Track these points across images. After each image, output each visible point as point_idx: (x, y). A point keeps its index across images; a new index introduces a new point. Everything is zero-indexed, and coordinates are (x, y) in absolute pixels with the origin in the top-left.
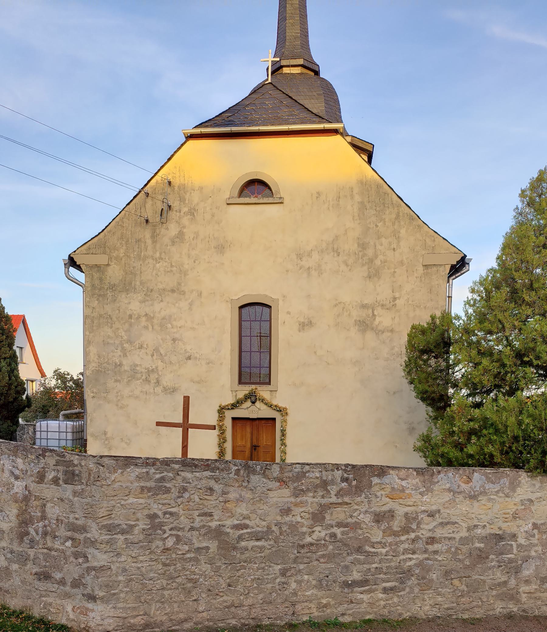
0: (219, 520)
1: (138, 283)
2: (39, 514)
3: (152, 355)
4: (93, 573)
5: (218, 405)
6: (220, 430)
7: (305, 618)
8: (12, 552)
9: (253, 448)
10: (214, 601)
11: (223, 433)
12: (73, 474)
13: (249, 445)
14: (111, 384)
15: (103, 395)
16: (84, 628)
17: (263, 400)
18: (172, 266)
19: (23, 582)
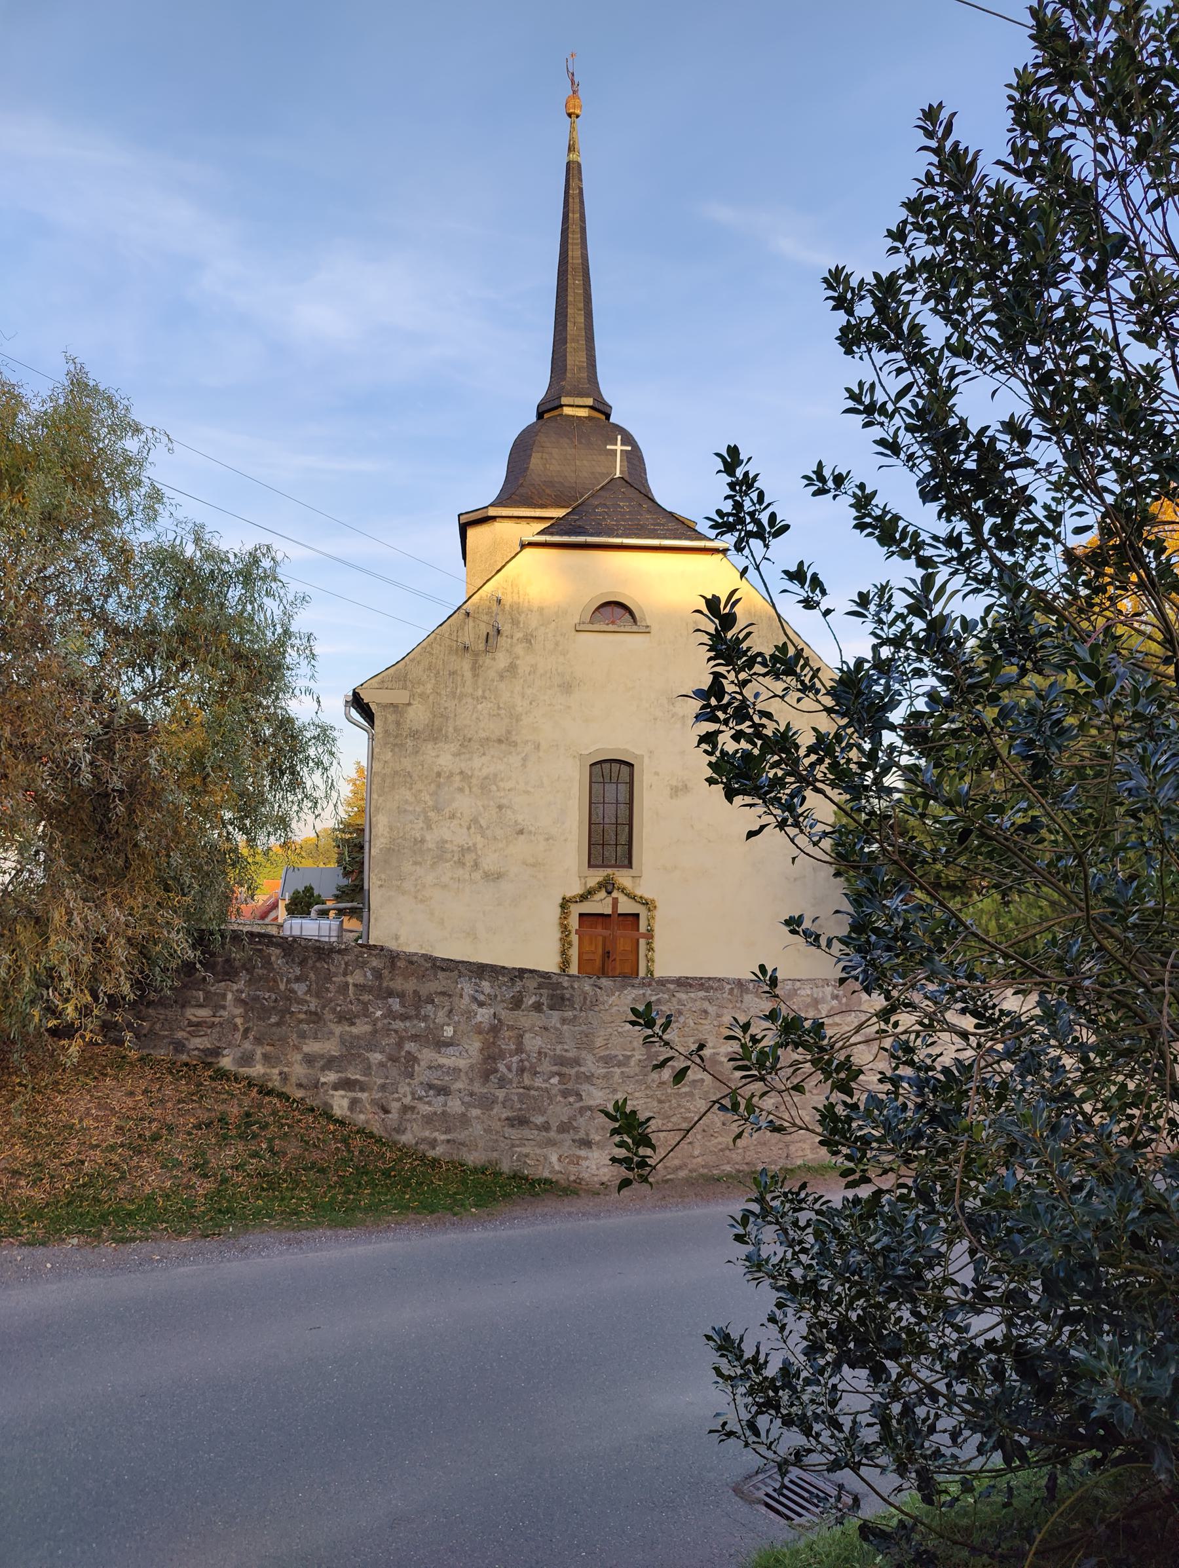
0: (714, 1048)
1: (451, 730)
2: (513, 1047)
3: (469, 828)
4: (589, 1113)
7: (799, 1162)
8: (471, 1095)
10: (708, 1144)
12: (563, 998)
13: (600, 951)
14: (407, 867)
15: (395, 883)
16: (575, 1181)
17: (623, 890)
18: (499, 708)
19: (488, 1130)
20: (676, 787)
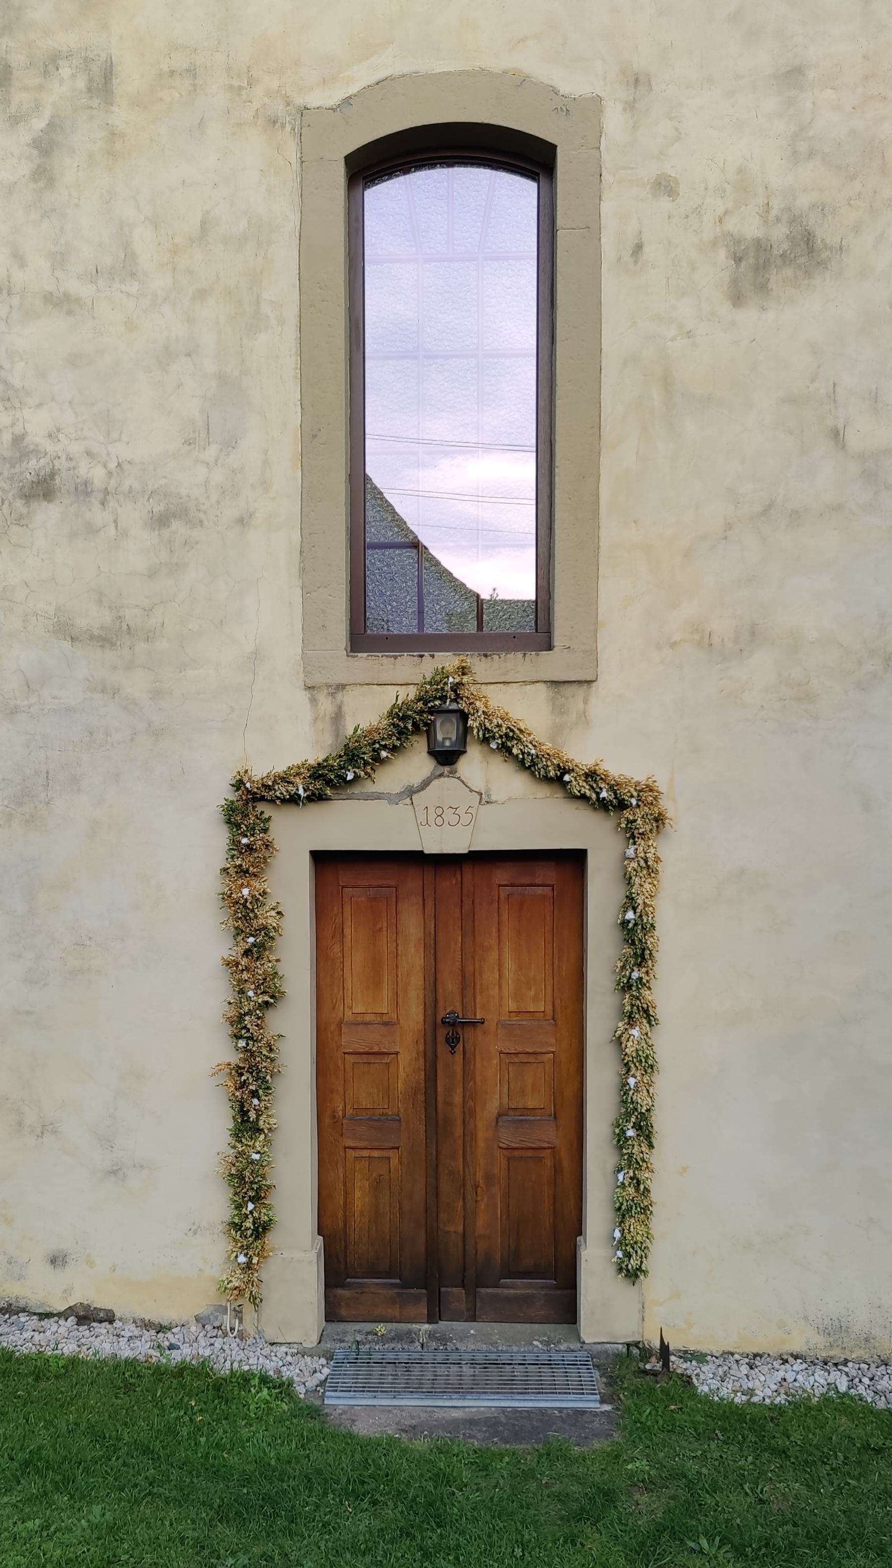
5: (230, 777)
6: (239, 931)
9: (442, 1033)
11: (261, 947)
20: (761, 247)
